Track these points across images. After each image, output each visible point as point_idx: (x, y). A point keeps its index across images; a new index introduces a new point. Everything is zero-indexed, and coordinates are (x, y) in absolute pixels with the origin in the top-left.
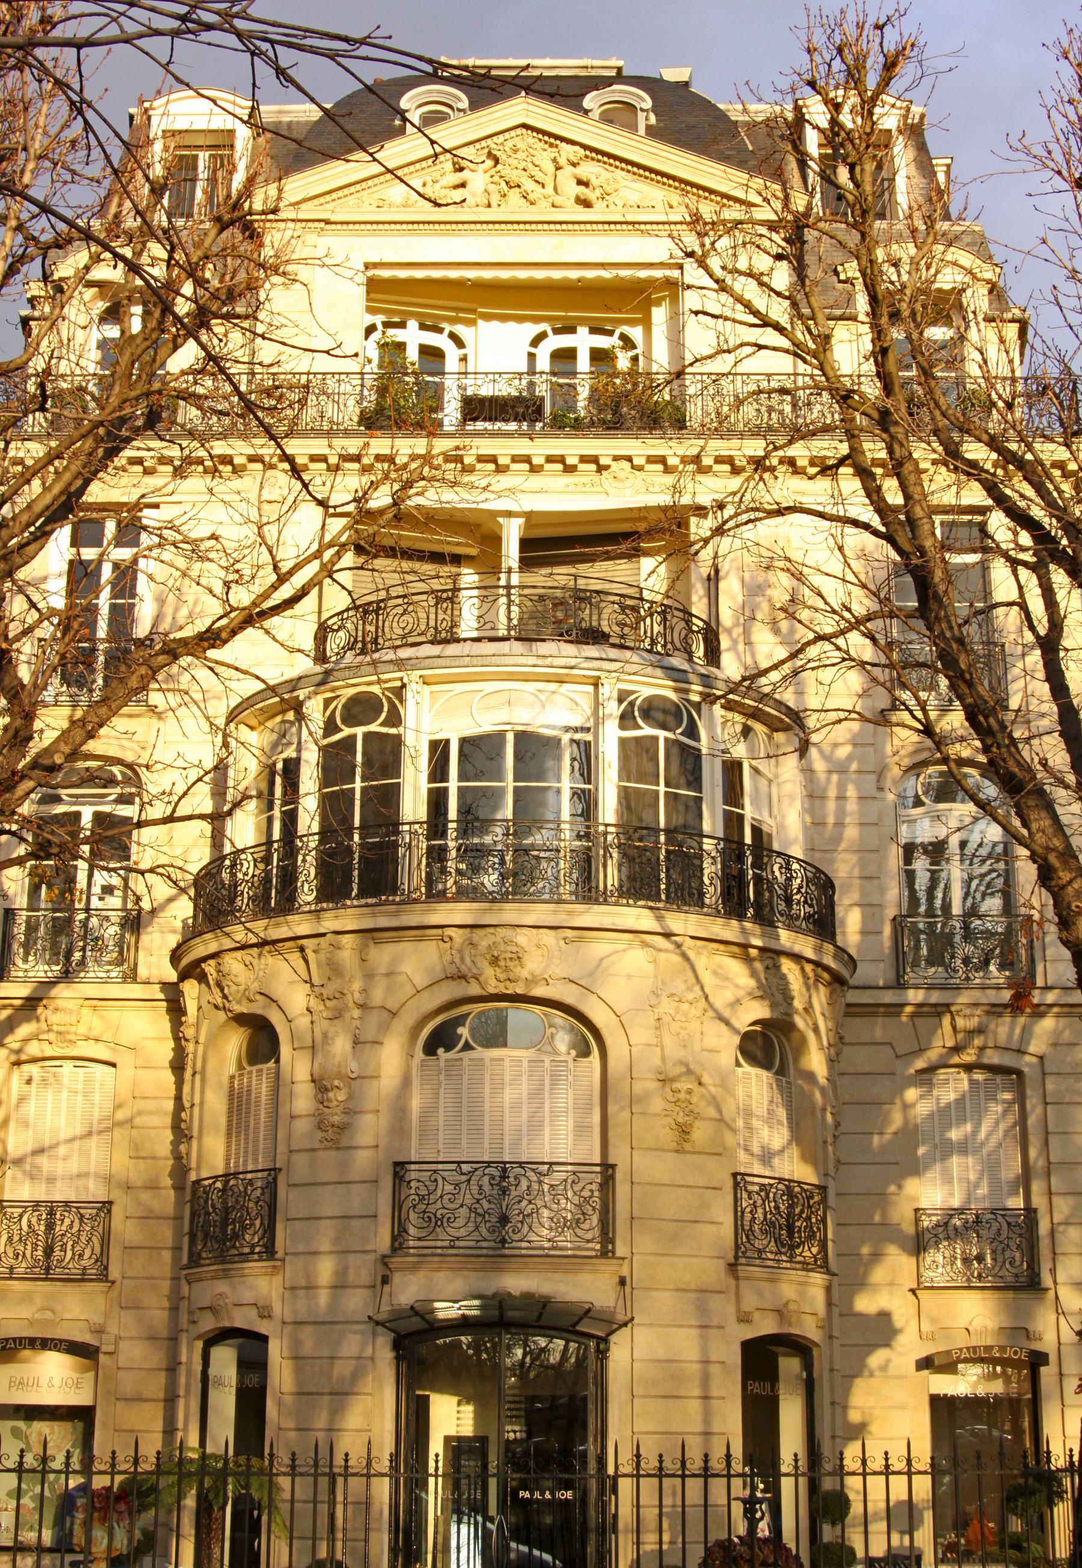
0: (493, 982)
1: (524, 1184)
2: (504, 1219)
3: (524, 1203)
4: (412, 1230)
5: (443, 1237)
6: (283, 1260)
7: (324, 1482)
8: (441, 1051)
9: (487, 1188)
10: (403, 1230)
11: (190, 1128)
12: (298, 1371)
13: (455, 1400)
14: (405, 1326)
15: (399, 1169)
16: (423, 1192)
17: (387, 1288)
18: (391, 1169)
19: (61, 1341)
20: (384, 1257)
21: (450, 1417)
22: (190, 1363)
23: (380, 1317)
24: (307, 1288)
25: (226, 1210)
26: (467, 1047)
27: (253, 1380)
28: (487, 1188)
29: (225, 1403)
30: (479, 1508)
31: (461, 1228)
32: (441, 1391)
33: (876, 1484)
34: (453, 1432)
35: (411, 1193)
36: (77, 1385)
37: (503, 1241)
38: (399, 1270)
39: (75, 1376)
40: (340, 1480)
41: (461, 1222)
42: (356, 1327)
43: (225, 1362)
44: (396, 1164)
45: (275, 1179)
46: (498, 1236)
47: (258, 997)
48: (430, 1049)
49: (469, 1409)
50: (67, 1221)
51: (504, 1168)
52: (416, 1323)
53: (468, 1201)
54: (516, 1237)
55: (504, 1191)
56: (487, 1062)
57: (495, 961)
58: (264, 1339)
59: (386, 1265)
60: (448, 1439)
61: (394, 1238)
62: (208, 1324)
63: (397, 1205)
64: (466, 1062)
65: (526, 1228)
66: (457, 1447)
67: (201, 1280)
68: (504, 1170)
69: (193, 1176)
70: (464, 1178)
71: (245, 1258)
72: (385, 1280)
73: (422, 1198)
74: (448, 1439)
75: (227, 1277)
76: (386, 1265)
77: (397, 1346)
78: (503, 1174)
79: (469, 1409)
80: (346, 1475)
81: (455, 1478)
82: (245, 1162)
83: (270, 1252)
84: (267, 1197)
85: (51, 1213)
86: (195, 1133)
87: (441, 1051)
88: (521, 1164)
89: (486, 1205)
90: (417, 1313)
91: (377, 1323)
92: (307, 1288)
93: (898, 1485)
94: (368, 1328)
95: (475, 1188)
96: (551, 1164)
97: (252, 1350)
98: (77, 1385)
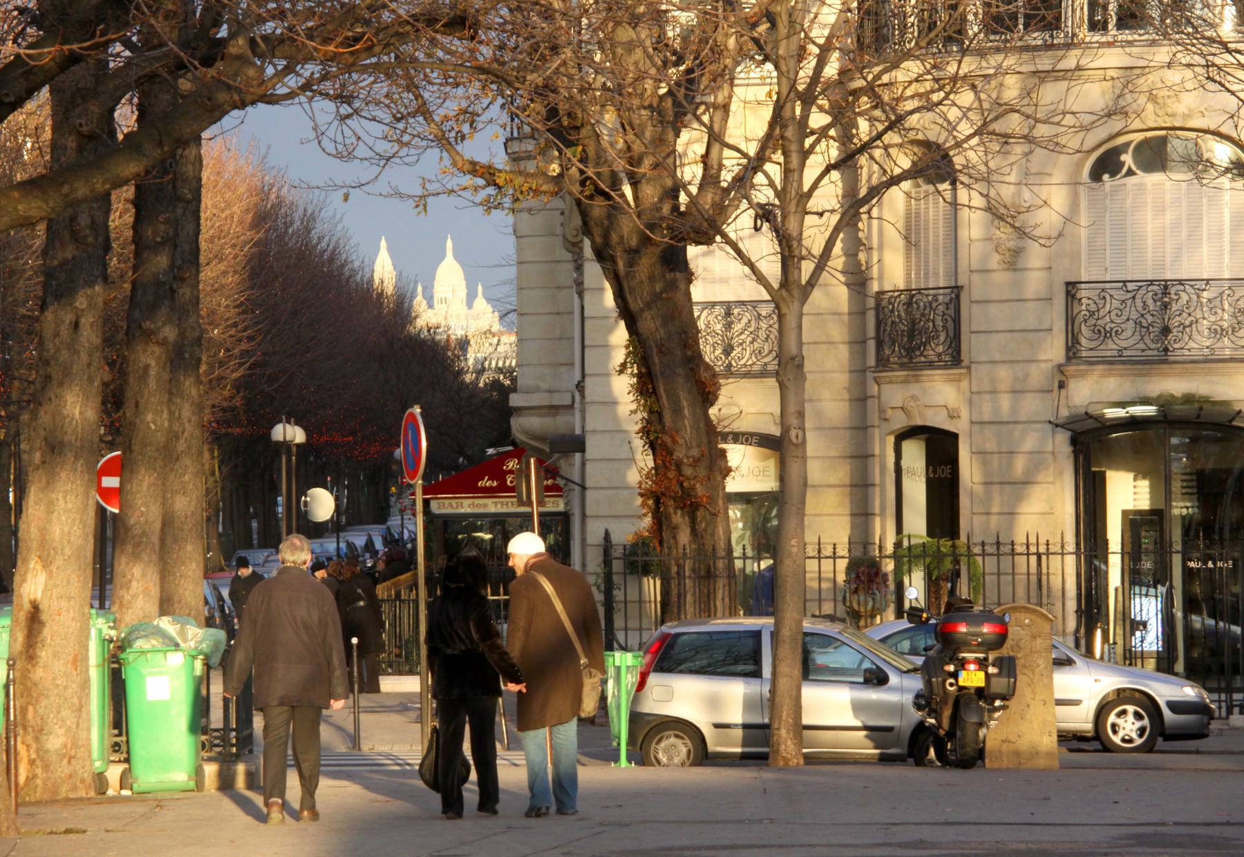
0: (1153, 117)
1: (1185, 297)
2: (1166, 331)
3: (1185, 315)
4: (1083, 341)
5: (1110, 348)
6: (969, 368)
7: (1033, 559)
8: (1106, 177)
9: (1150, 302)
10: (1076, 341)
11: (869, 237)
12: (985, 465)
13: (1131, 475)
14: (1080, 427)
15: (1071, 289)
16: (1093, 307)
17: (1063, 392)
18: (1064, 288)
19: (752, 435)
20: (1060, 366)
21: (1126, 492)
22: (883, 456)
23: (1060, 421)
24: (991, 392)
25: (913, 323)
26: (1130, 173)
27: (945, 472)
28: (1150, 302)
29: (916, 491)
30: (1161, 576)
31: (1128, 340)
32: (1117, 467)
33: (827, 565)
34: (1130, 506)
35: (1082, 310)
36: (763, 472)
37: (1166, 350)
38: (1074, 376)
39: (761, 465)
40: (1044, 558)
41: (1129, 333)
42: (1038, 426)
43: (915, 455)
44: (1068, 284)
45: (958, 297)
46: (1159, 346)
47: (933, 126)
48: (1096, 175)
49: (1144, 485)
50: (745, 320)
51: (1165, 286)
52: (1091, 424)
53: (1134, 315)
54: (1176, 346)
55: (1166, 306)
56: (1149, 187)
57: (1152, 98)
58: (954, 437)
59: (1062, 372)
60: (1125, 513)
61: (1068, 349)
62: (900, 422)
63: (1070, 320)
64: (1129, 187)
65: (1186, 338)
66: (1135, 523)
67: (891, 382)
68: (1166, 287)
69: (875, 287)
70: (1130, 295)
71: (931, 365)
72: (1062, 386)
73: (1092, 314)
74: (1125, 513)
75: (917, 381)
76: (1062, 372)
77: (1074, 441)
78: (1164, 290)
79: (1144, 485)
80: (1048, 554)
81: (1132, 553)
82: (926, 280)
83: (956, 361)
84: (951, 312)
85: (728, 314)
86: (875, 243)
87: (1106, 177)
88: (1181, 282)
89: (1150, 319)
90: (1091, 417)
91: (1057, 426)
92: (991, 392)
93: (827, 565)
94: (1049, 427)
95: (1139, 304)
96: (1208, 280)
97: (941, 448)
98: (763, 472)
